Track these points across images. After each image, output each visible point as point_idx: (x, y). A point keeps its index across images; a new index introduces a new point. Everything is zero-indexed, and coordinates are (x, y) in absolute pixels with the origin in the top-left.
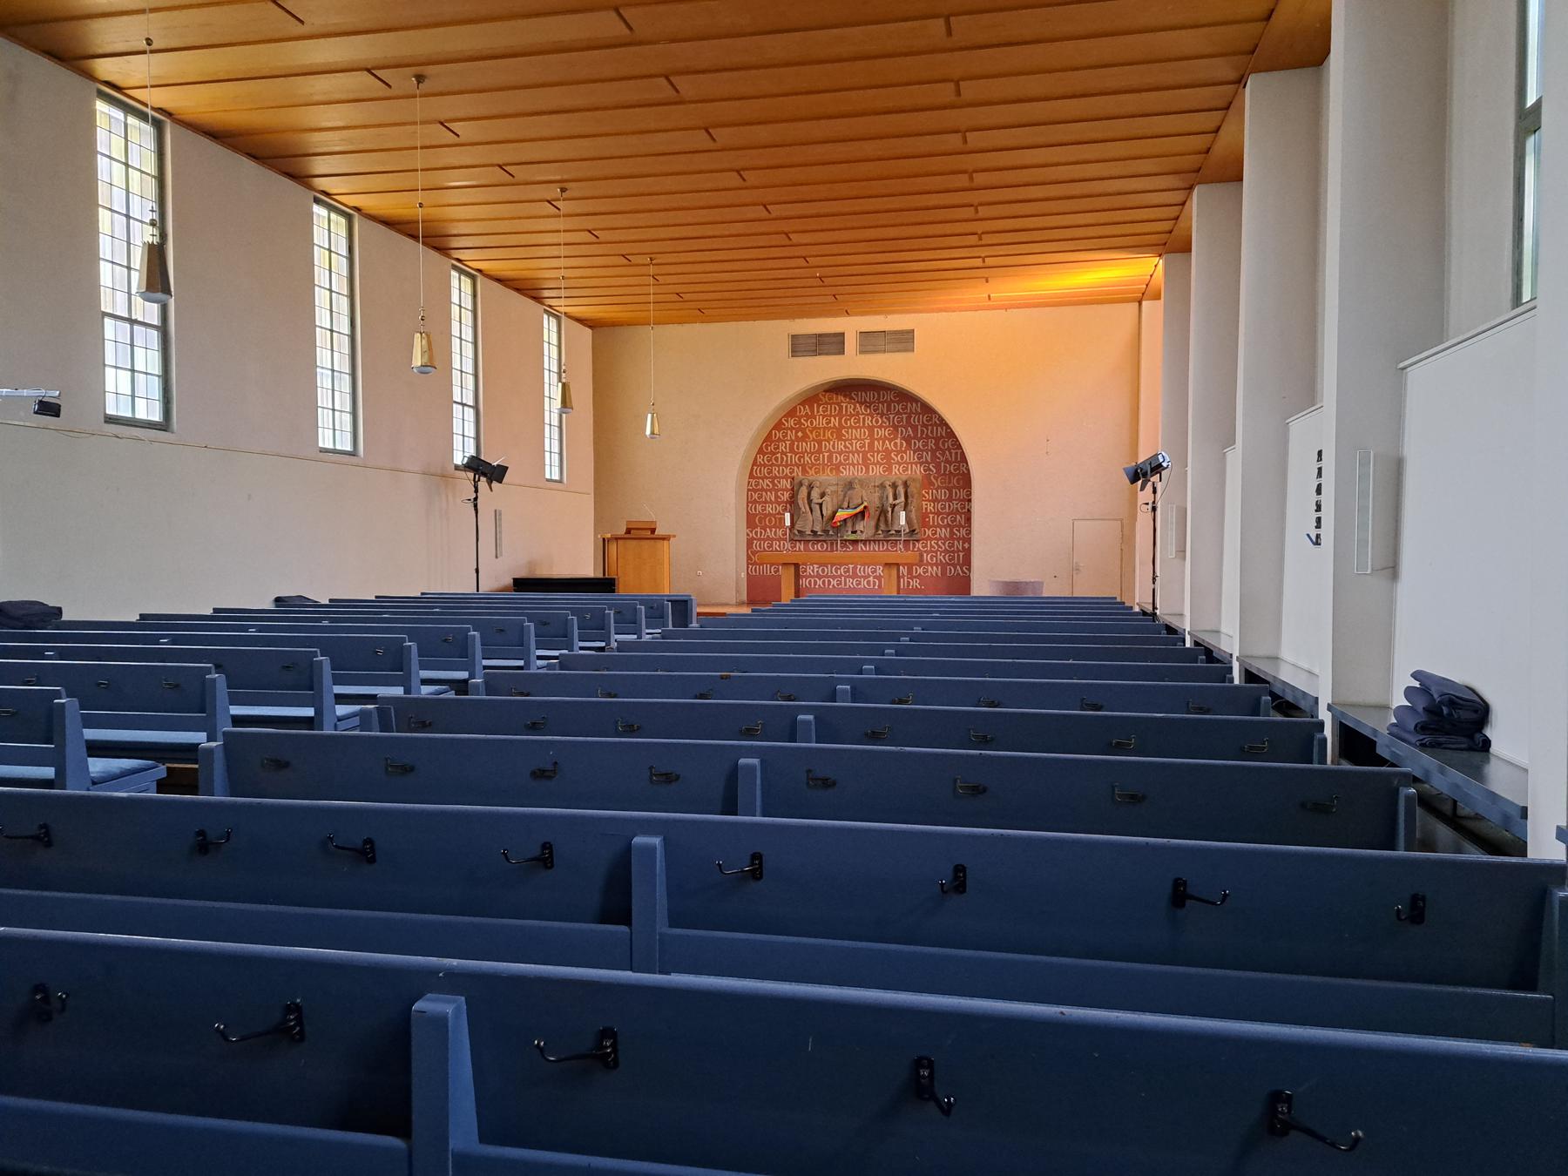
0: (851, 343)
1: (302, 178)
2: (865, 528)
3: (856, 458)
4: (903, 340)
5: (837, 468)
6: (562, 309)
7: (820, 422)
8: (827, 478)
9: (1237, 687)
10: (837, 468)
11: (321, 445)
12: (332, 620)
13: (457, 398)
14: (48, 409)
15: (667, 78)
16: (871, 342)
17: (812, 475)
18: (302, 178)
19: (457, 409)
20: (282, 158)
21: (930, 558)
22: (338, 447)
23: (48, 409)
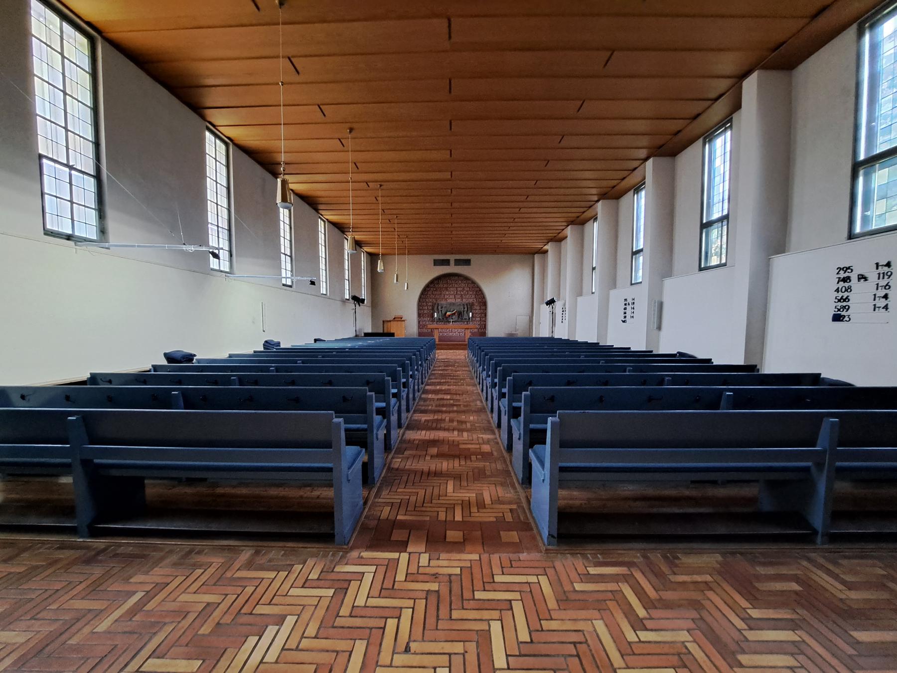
0: (452, 262)
1: (198, 109)
2: (455, 318)
3: (452, 297)
4: (467, 262)
5: (446, 299)
6: (327, 217)
7: (441, 285)
8: (443, 302)
9: (409, 342)
10: (446, 299)
11: (212, 266)
12: (635, 369)
13: (283, 251)
14: (313, 283)
15: (289, 59)
16: (458, 262)
17: (438, 302)
18: (198, 109)
19: (283, 256)
20: (183, 90)
21: (474, 326)
22: (222, 269)
23: (313, 283)
